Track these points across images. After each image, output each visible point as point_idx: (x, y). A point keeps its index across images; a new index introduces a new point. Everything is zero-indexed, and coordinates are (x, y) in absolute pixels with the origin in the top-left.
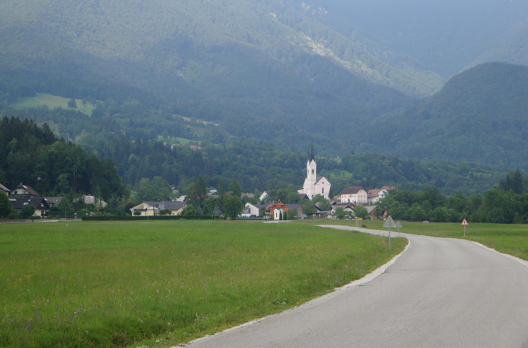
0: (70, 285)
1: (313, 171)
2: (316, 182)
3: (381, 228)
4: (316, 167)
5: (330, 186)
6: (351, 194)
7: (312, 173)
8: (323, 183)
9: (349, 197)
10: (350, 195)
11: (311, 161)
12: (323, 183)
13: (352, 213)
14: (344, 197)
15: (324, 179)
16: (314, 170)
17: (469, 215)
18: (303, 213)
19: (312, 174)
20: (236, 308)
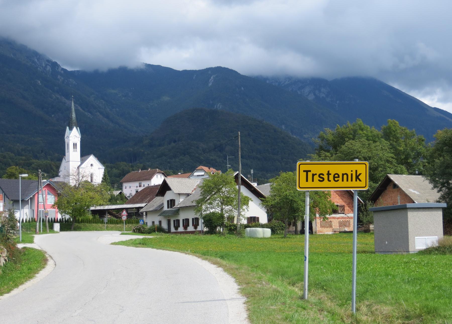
0: (78, 199)
1: (75, 145)
2: (79, 163)
3: (325, 161)
4: (80, 139)
5: (103, 170)
6: (140, 182)
7: (74, 148)
8: (92, 165)
9: (137, 187)
10: (140, 184)
11: (71, 129)
12: (92, 165)
13: (353, 135)
14: (128, 187)
15: (92, 159)
16: (76, 144)
17: (404, 152)
18: (58, 208)
19: (74, 151)
20: (265, 181)
